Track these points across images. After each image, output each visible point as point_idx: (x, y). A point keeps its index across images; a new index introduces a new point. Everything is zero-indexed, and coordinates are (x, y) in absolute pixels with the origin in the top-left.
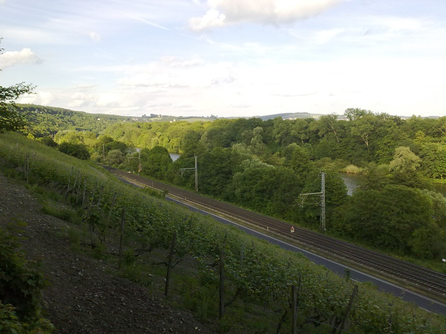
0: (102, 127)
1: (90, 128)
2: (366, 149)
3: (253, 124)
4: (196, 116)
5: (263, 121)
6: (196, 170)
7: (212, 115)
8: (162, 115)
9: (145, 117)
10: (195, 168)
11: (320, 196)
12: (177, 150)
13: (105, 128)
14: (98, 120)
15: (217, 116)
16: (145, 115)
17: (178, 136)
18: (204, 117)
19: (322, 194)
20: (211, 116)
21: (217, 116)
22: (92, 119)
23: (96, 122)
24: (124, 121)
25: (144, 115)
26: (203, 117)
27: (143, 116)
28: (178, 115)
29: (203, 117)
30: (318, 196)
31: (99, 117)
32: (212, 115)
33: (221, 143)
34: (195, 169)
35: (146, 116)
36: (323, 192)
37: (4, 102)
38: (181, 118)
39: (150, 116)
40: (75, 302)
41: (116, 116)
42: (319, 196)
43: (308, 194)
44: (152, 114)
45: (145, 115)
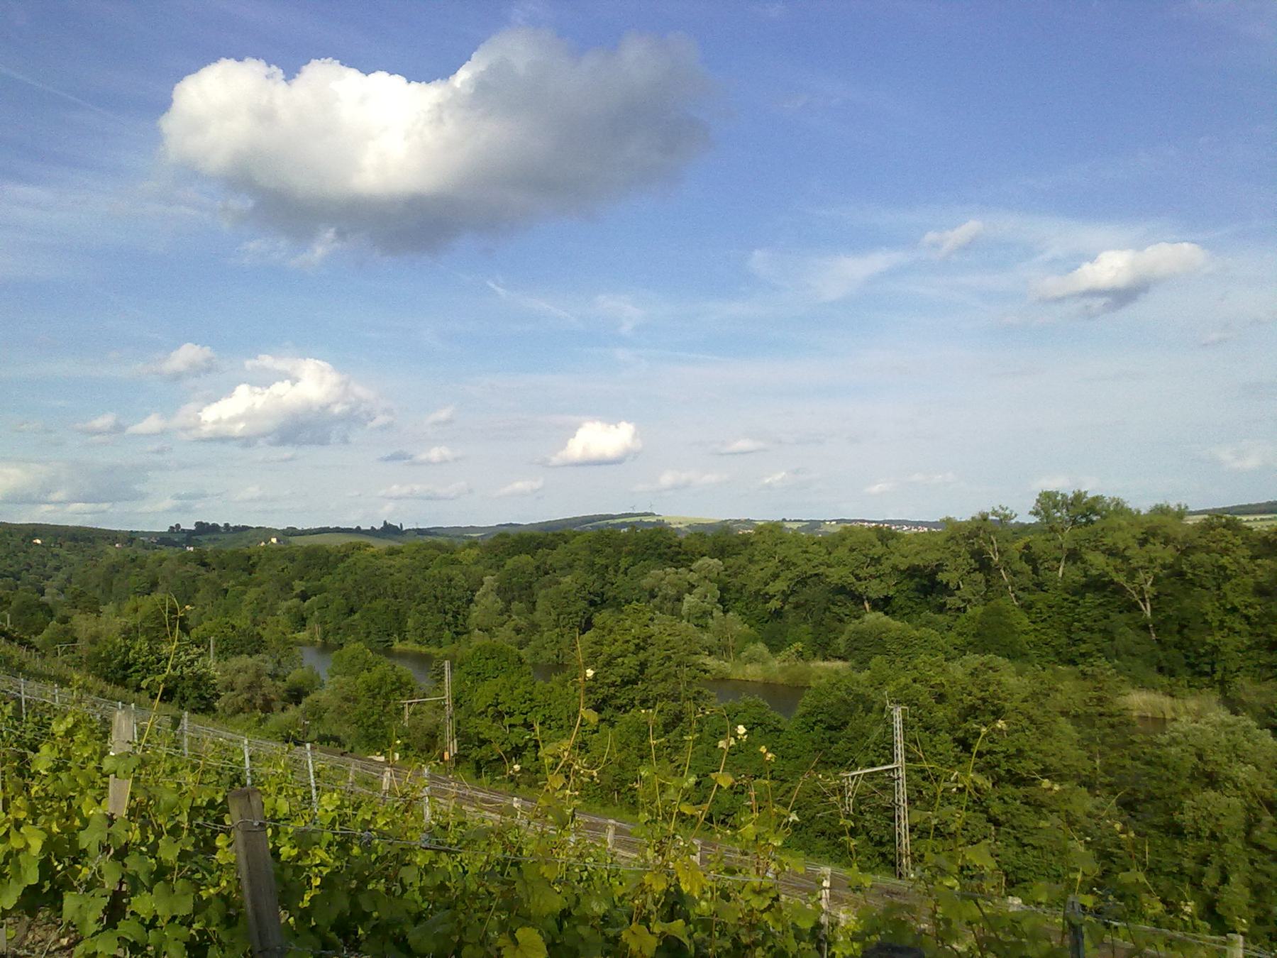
0: (50, 564)
1: (11, 569)
2: (1145, 628)
3: (662, 550)
4: (337, 528)
5: (1143, 512)
6: (447, 703)
7: (385, 523)
8: (232, 525)
9: (178, 532)
10: (446, 697)
11: (891, 775)
12: (387, 641)
13: (57, 569)
14: (37, 544)
15: (401, 525)
16: (178, 526)
17: (380, 594)
18: (363, 528)
19: (897, 769)
20: (382, 525)
21: (401, 525)
22: (17, 539)
23: (31, 550)
24: (117, 545)
25: (174, 525)
26: (359, 528)
27: (171, 527)
28: (282, 526)
29: (359, 528)
30: (886, 775)
31: (36, 536)
32: (385, 523)
33: (571, 613)
34: (444, 700)
35: (183, 530)
36: (899, 765)
37: (907, 903)
38: (292, 532)
39: (193, 528)
40: (87, 890)
41: (92, 531)
42: (890, 777)
43: (863, 772)
44: (201, 523)
45: (178, 526)
